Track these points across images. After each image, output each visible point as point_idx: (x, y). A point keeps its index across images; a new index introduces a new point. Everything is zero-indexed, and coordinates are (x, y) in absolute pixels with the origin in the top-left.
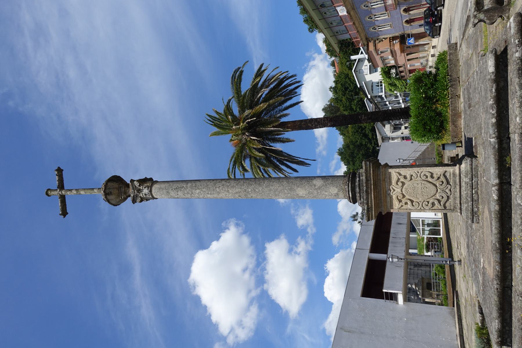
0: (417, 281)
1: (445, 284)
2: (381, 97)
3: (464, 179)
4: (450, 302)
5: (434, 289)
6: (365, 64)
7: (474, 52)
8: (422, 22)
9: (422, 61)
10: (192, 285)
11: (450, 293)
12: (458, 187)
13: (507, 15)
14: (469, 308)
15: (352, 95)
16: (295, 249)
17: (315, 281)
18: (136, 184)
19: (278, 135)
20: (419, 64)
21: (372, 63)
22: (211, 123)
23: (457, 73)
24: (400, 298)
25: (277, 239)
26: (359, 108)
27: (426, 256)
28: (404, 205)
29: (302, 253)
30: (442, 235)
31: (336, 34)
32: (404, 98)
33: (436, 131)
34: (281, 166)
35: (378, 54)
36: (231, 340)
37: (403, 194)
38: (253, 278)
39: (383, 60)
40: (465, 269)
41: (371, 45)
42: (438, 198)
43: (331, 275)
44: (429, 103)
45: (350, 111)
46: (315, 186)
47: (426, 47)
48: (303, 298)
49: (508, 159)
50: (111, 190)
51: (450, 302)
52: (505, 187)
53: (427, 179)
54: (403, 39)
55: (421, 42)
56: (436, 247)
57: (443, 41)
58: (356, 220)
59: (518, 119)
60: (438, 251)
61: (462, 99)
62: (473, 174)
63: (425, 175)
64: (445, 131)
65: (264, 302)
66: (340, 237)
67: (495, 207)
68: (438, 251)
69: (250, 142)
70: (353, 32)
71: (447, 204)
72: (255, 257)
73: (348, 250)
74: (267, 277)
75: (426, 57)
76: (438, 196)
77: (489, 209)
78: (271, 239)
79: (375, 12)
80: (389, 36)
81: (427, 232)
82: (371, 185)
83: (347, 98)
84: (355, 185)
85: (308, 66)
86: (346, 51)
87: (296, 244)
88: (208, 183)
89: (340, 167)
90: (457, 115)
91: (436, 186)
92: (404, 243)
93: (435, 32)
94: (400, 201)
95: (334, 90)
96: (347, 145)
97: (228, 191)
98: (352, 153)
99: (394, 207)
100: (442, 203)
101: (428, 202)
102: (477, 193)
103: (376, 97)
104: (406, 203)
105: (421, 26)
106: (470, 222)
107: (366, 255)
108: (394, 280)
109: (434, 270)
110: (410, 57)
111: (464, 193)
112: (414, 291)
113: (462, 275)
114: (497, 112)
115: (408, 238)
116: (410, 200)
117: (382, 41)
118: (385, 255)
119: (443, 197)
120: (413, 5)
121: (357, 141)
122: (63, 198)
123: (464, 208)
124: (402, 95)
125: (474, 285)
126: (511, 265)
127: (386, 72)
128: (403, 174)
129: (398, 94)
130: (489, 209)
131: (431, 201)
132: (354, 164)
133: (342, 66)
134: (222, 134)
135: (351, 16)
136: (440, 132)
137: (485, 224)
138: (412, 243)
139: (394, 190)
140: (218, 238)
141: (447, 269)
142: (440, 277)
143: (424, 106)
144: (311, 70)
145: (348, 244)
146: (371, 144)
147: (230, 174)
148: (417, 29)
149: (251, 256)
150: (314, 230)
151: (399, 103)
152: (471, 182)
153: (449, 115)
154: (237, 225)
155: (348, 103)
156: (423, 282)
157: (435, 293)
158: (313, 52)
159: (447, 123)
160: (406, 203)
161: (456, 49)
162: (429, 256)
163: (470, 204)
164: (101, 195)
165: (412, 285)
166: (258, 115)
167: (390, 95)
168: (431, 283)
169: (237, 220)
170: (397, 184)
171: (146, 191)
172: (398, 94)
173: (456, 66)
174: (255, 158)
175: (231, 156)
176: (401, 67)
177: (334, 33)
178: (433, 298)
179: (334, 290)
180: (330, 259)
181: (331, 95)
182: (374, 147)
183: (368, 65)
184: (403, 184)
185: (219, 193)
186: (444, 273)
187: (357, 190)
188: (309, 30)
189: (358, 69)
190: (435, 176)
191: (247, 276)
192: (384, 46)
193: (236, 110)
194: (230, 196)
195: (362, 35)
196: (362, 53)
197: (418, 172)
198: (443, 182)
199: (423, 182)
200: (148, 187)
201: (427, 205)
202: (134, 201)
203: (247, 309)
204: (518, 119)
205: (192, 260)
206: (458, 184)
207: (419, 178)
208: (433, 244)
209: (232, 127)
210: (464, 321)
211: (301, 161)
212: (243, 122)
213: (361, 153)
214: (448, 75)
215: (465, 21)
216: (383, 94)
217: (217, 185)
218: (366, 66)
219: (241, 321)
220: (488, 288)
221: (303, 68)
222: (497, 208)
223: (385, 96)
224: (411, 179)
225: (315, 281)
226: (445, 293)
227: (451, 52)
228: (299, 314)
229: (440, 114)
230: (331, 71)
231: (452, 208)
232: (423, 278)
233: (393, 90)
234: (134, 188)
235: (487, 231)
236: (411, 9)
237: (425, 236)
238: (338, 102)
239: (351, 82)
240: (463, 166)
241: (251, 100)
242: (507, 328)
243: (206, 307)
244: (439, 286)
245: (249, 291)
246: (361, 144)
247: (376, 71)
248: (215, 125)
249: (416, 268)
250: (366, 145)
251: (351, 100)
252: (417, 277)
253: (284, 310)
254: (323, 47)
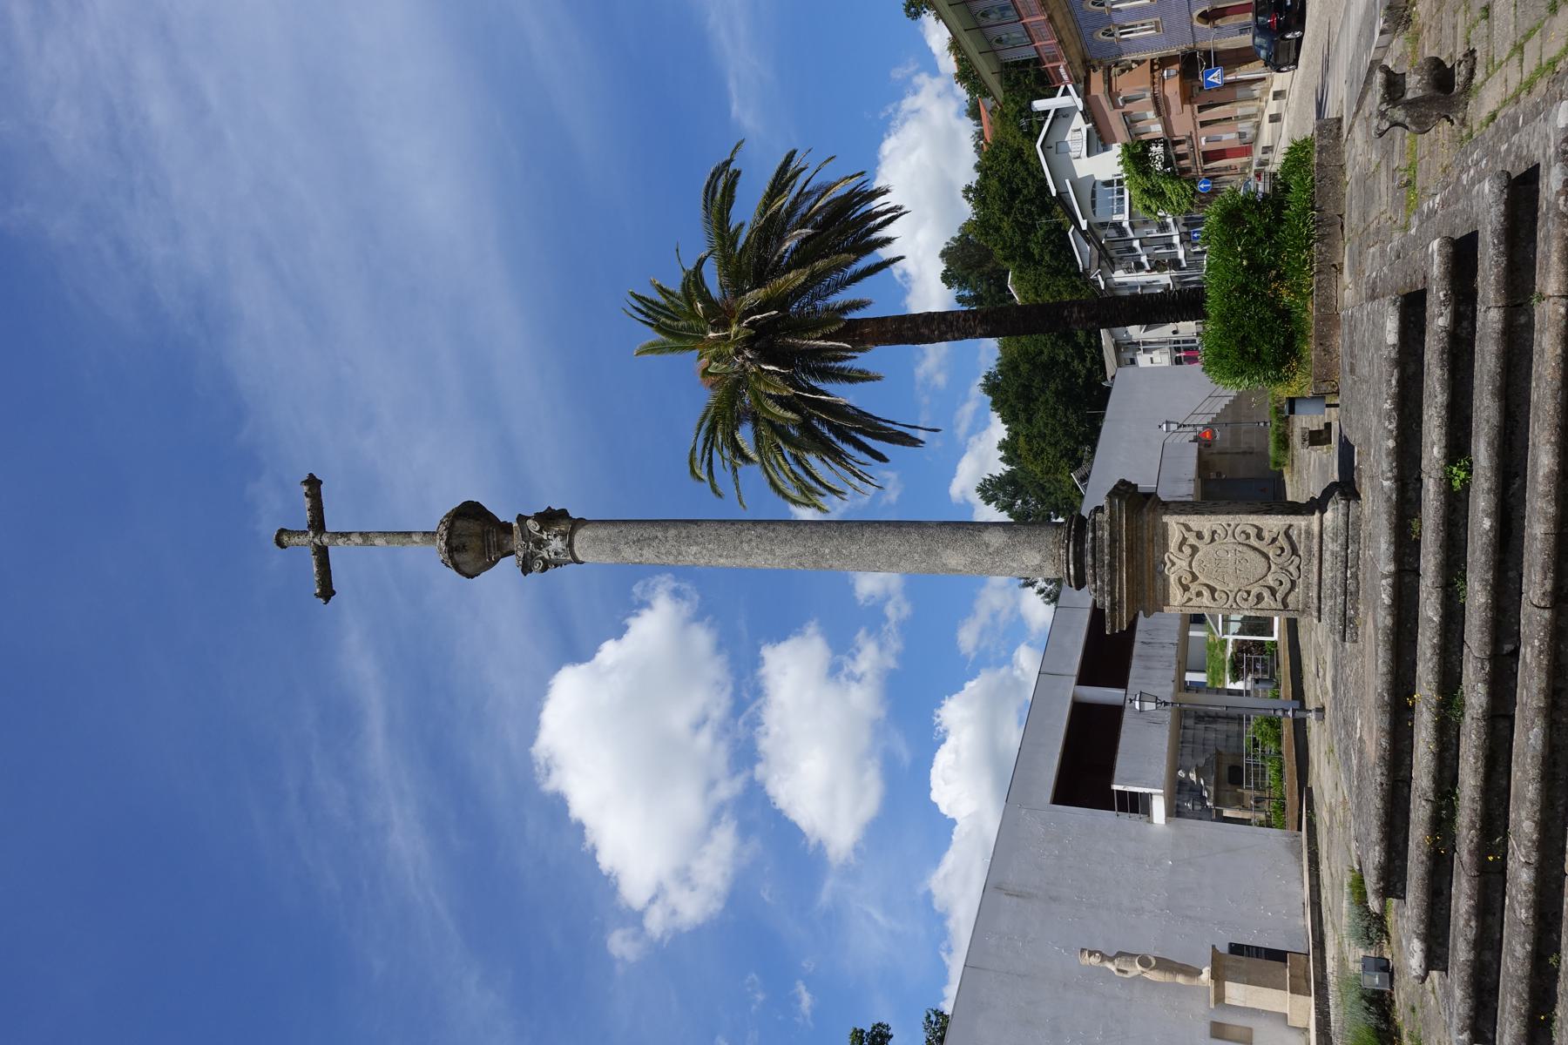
0: (1202, 762)
1: (1280, 771)
2: (1118, 226)
4: (1291, 818)
5: (1248, 782)
6: (1073, 127)
7: (1384, 162)
8: (1249, 17)
9: (1244, 126)
10: (542, 763)
11: (1291, 795)
12: (1316, 562)
13: (1460, 115)
14: (1338, 831)
15: (1030, 213)
16: (849, 666)
17: (906, 756)
18: (533, 526)
19: (836, 359)
20: (1233, 136)
21: (1095, 125)
22: (642, 317)
23: (1338, 202)
24: (1159, 807)
25: (796, 634)
26: (1051, 252)
27: (1231, 692)
29: (869, 677)
30: (1277, 634)
31: (999, 46)
32: (1185, 229)
33: (1274, 360)
34: (840, 443)
35: (1116, 106)
36: (655, 922)
37: (1193, 573)
38: (722, 748)
39: (1130, 122)
41: (1097, 79)
42: (1271, 583)
43: (951, 741)
44: (1259, 283)
45: (1039, 300)
46: (987, 546)
47: (1257, 89)
49: (1415, 523)
50: (463, 539)
51: (1291, 818)
52: (1407, 579)
54: (1190, 64)
55: (1243, 73)
56: (1259, 667)
57: (1304, 85)
58: (1032, 584)
59: (1436, 450)
60: (1264, 680)
61: (1346, 277)
62: (1350, 533)
64: (1299, 361)
65: (756, 815)
66: (982, 634)
67: (1385, 620)
68: (1264, 680)
69: (758, 378)
70: (1047, 43)
71: (1291, 599)
72: (730, 689)
73: (1004, 671)
74: (764, 744)
75: (1255, 115)
77: (1375, 621)
78: (780, 634)
80: (1148, 56)
81: (1235, 627)
82: (1121, 551)
83: (1016, 221)
84: (1082, 550)
85: (896, 110)
86: (1017, 78)
87: (852, 650)
88: (722, 531)
89: (987, 424)
90: (1330, 318)
91: (1268, 558)
92: (1174, 660)
93: (1283, 55)
94: (1186, 588)
95: (977, 194)
96: (1011, 362)
97: (772, 552)
98: (1027, 387)
99: (1172, 602)
101: (1249, 593)
102: (1355, 576)
103: (1104, 225)
104: (1199, 594)
105: (1242, 31)
106: (1337, 638)
107: (1068, 690)
108: (1142, 761)
109: (1249, 732)
110: (1207, 115)
113: (1324, 748)
114: (1398, 427)
115: (1185, 638)
117: (1131, 69)
118: (1121, 692)
121: (1042, 352)
122: (322, 554)
123: (1326, 609)
124: (1181, 220)
125: (1341, 778)
126: (1412, 737)
127: (1137, 157)
129: (1170, 220)
130: (1376, 618)
131: (1255, 591)
132: (1029, 421)
133: (1003, 124)
134: (673, 350)
136: (1285, 361)
137: (1368, 648)
138: (1194, 653)
139: (1173, 564)
140: (619, 632)
141: (1287, 730)
142: (1267, 749)
143: (1244, 288)
144: (907, 125)
145: (1003, 653)
146: (1083, 360)
147: (697, 463)
148: (1234, 36)
149: (717, 683)
150: (906, 609)
151: (1170, 245)
153: (1309, 319)
154: (677, 594)
155: (1018, 238)
156: (1218, 764)
157: (1249, 794)
158: (912, 69)
159: (1304, 340)
160: (1199, 594)
161: (1338, 136)
162: (1240, 693)
163: (1340, 600)
164: (435, 551)
165: (1187, 772)
166: (780, 302)
167: (1146, 222)
168: (1237, 769)
169: (676, 580)
170: (1180, 550)
171: (557, 544)
172: (1170, 220)
173: (1335, 183)
174: (770, 423)
175: (701, 414)
176: (1180, 142)
177: (989, 42)
178: (1245, 808)
179: (963, 787)
180: (950, 695)
181: (967, 211)
182: (1089, 371)
183: (1084, 127)
184: (1194, 549)
185: (748, 555)
186: (1278, 739)
187: (1089, 559)
188: (907, 10)
189: (1052, 142)
190: (1266, 534)
191: (704, 740)
192: (1133, 84)
193: (713, 281)
194: (777, 563)
195: (1073, 50)
196: (1066, 92)
198: (1283, 550)
199: (1240, 548)
200: (563, 535)
202: (545, 569)
203: (705, 835)
204: (1436, 450)
205: (540, 691)
207: (1230, 539)
208: (1251, 658)
209: (705, 333)
210: (1324, 867)
211: (900, 433)
212: (740, 322)
213: (1052, 386)
214: (1313, 208)
216: (1124, 219)
217: (745, 536)
218: (1077, 132)
219: (687, 869)
220: (1366, 783)
221: (882, 115)
222: (1389, 621)
223: (1131, 224)
224: (1213, 540)
226: (1278, 794)
227: (1325, 142)
228: (856, 850)
229: (1285, 314)
230: (966, 130)
232: (1218, 753)
233: (1154, 207)
234: (527, 536)
235: (1370, 666)
237: (1231, 638)
238: (987, 234)
239: (1030, 173)
240: (1329, 515)
241: (759, 257)
242: (1398, 863)
243: (580, 827)
244: (1264, 774)
245: (712, 784)
246: (1053, 360)
247: (1106, 148)
248: (660, 329)
249: (1201, 726)
250: (1065, 362)
251: (1026, 229)
252: (1204, 751)
253: (813, 841)
254: (949, 64)
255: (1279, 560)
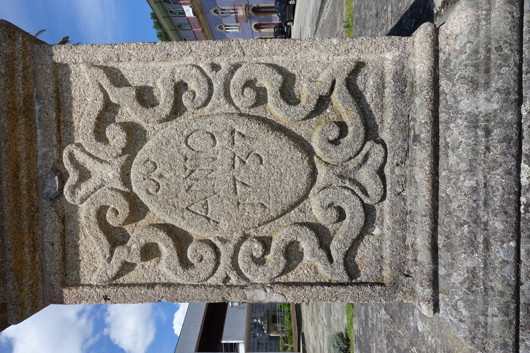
0: (262, 314)
1: (290, 319)
3: (465, 104)
5: (279, 321)
11: (295, 332)
12: (422, 154)
17: (164, 317)
28: (135, 259)
31: (171, 14)
38: (91, 322)
40: (313, 310)
48: (150, 338)
53: (259, 111)
63: (249, 83)
71: (364, 254)
74: (108, 320)
76: (316, 210)
79: (226, 22)
91: (309, 152)
94: (116, 238)
100: (337, 248)
101: (266, 243)
111: (457, 192)
112: (259, 326)
113: (309, 317)
116: (170, 230)
119: (341, 215)
120: (264, 23)
123: (454, 278)
128: (136, 81)
131: (281, 235)
135: (199, 21)
139: (84, 175)
152: (510, 116)
157: (279, 325)
160: (149, 252)
163: (501, 252)
165: (257, 320)
170: (99, 135)
177: (175, 27)
190: (304, 90)
191: (83, 321)
197: (215, 67)
201: (260, 262)
206: (425, 135)
215: (318, 10)
224: (177, 109)
225: (164, 317)
226: (289, 329)
231: (387, 273)
232: (268, 310)
236: (262, 27)
245: (86, 340)
255: (337, 155)
